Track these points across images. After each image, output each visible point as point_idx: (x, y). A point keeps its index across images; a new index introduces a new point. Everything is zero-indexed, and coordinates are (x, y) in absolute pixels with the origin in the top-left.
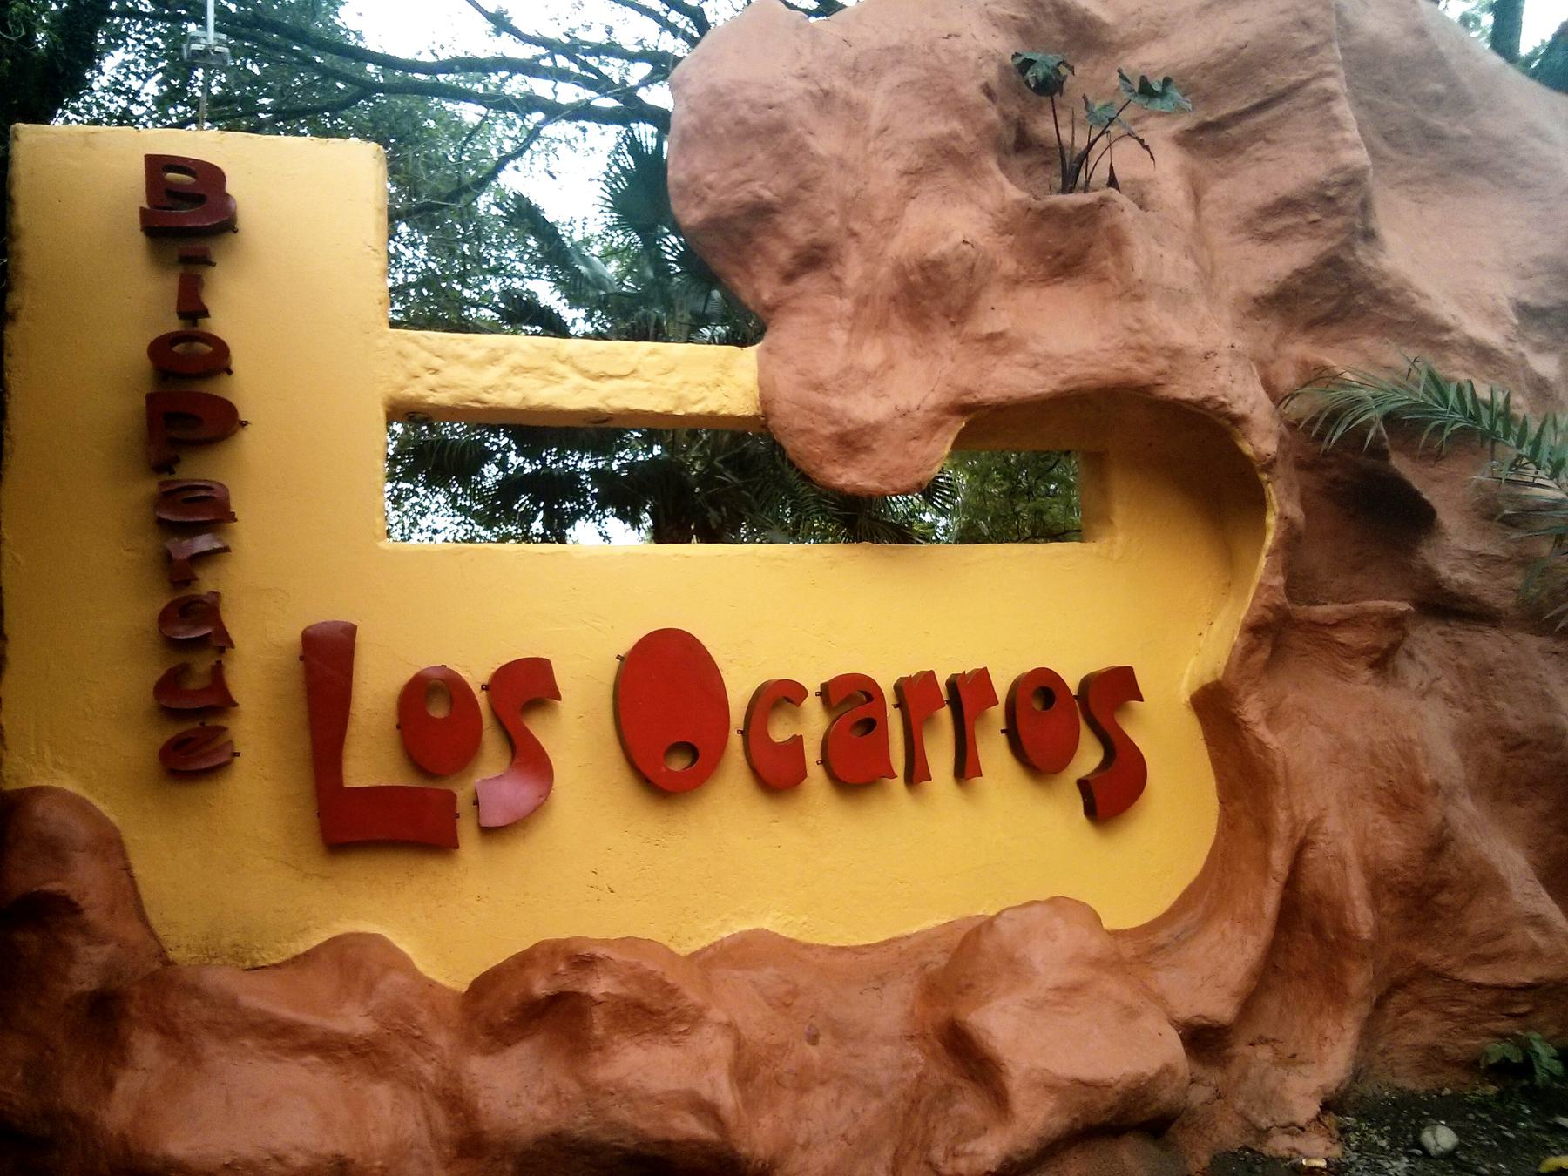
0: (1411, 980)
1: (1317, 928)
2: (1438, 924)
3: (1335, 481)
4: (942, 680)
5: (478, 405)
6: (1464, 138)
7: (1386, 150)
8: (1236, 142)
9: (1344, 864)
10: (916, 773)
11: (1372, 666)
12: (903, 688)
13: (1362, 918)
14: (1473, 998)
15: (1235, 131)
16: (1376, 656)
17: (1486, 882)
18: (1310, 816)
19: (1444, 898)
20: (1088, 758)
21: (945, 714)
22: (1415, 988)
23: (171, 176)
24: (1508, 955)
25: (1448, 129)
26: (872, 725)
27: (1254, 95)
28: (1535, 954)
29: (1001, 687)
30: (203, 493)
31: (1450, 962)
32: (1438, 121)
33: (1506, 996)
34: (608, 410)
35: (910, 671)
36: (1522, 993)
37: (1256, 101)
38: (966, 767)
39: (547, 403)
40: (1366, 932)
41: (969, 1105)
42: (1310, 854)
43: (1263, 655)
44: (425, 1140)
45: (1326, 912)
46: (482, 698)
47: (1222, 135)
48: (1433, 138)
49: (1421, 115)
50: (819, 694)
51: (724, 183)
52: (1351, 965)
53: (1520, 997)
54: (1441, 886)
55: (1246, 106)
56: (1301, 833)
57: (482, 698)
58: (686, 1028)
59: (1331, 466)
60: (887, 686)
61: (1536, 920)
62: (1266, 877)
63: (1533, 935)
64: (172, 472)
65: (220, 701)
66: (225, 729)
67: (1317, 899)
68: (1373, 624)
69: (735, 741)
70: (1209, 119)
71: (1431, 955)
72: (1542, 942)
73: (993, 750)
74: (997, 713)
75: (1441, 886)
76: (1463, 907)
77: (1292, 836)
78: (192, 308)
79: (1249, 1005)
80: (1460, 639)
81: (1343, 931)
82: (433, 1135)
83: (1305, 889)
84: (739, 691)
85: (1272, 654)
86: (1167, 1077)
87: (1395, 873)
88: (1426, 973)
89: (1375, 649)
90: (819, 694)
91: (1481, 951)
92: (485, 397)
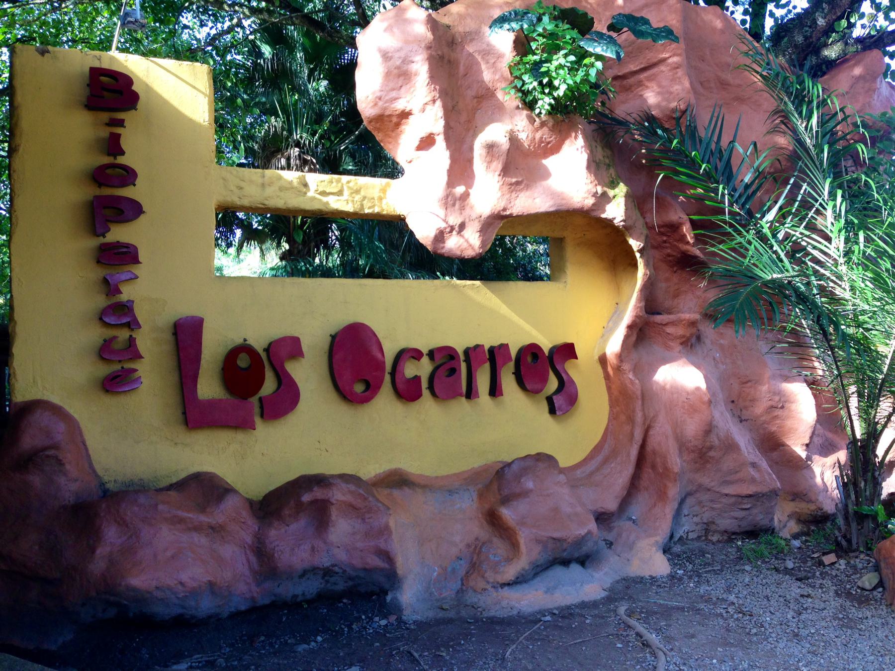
0: (696, 491)
1: (654, 467)
2: (708, 466)
3: (669, 255)
4: (487, 348)
5: (262, 206)
6: (739, 86)
7: (701, 90)
8: (631, 86)
9: (667, 437)
10: (471, 393)
11: (681, 344)
12: (467, 352)
13: (676, 462)
14: (724, 500)
15: (631, 81)
16: (684, 339)
17: (731, 446)
18: (652, 415)
19: (712, 453)
20: (553, 384)
21: (487, 366)
22: (698, 495)
23: (103, 78)
24: (742, 480)
25: (732, 82)
26: (453, 371)
27: (642, 63)
28: (753, 480)
29: (513, 352)
30: (125, 250)
31: (713, 484)
32: (728, 77)
33: (740, 499)
34: (327, 210)
35: (471, 344)
36: (747, 499)
37: (643, 66)
38: (495, 391)
39: (296, 206)
40: (676, 469)
41: (499, 548)
42: (651, 432)
43: (634, 338)
44: (247, 573)
45: (658, 460)
46: (263, 355)
47: (625, 82)
48: (724, 85)
49: (719, 74)
50: (427, 355)
51: (387, 98)
52: (670, 485)
53: (746, 500)
54: (711, 448)
55: (638, 68)
56: (648, 422)
57: (263, 355)
58: (128, 320)
59: (667, 248)
60: (460, 351)
61: (754, 465)
62: (632, 443)
63: (752, 472)
64: (104, 237)
65: (132, 351)
66: (135, 370)
67: (654, 452)
68: (684, 325)
69: (387, 378)
70: (620, 74)
71: (705, 480)
72: (757, 475)
73: (508, 382)
74: (511, 365)
75: (711, 448)
76: (720, 458)
77: (644, 424)
78: (114, 146)
79: (625, 502)
80: (722, 331)
81: (666, 469)
82: (251, 569)
83: (649, 448)
84: (390, 351)
85: (637, 340)
86: (589, 536)
87: (690, 441)
88: (700, 488)
89: (684, 336)
90: (427, 355)
91: (728, 479)
92: (266, 202)
